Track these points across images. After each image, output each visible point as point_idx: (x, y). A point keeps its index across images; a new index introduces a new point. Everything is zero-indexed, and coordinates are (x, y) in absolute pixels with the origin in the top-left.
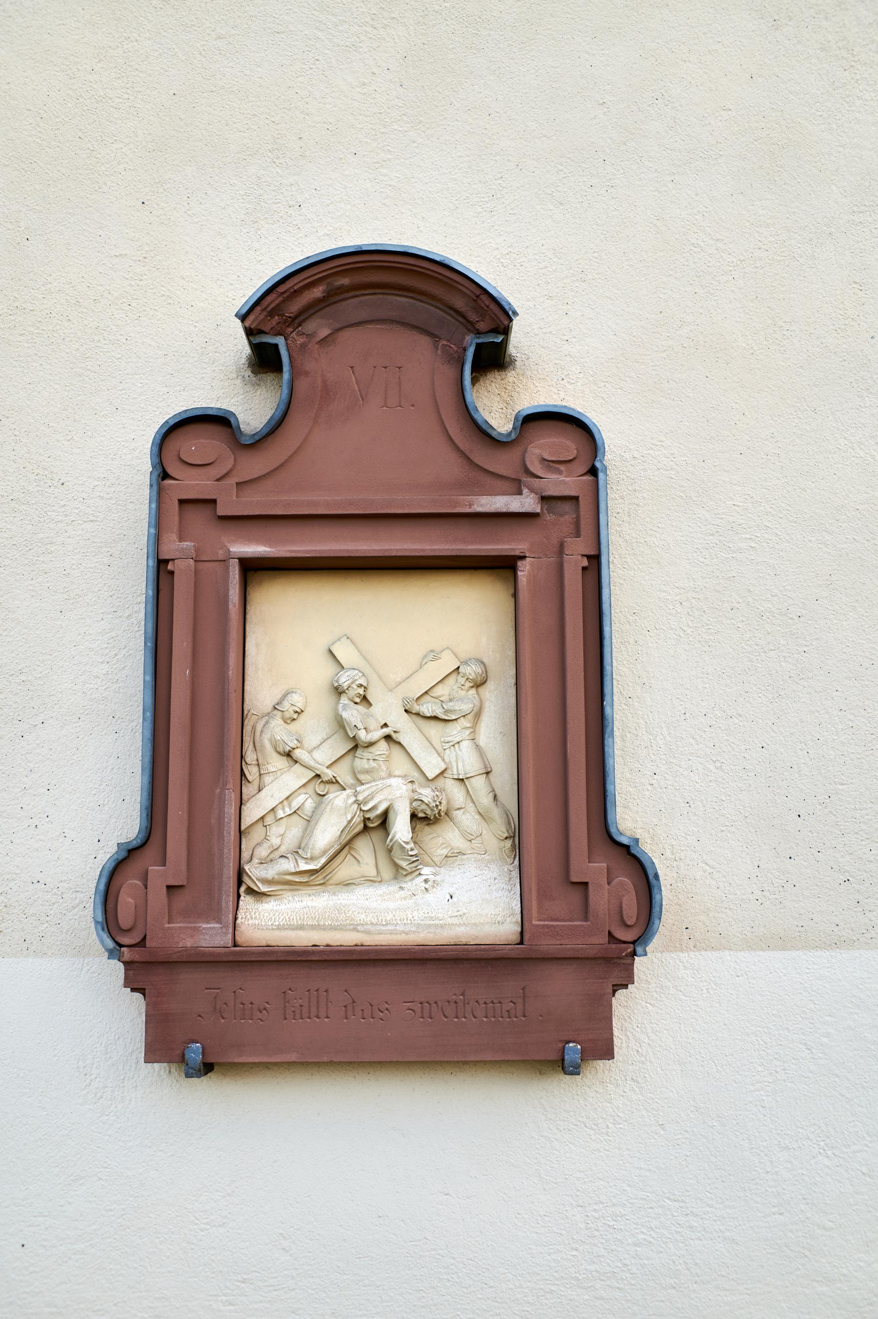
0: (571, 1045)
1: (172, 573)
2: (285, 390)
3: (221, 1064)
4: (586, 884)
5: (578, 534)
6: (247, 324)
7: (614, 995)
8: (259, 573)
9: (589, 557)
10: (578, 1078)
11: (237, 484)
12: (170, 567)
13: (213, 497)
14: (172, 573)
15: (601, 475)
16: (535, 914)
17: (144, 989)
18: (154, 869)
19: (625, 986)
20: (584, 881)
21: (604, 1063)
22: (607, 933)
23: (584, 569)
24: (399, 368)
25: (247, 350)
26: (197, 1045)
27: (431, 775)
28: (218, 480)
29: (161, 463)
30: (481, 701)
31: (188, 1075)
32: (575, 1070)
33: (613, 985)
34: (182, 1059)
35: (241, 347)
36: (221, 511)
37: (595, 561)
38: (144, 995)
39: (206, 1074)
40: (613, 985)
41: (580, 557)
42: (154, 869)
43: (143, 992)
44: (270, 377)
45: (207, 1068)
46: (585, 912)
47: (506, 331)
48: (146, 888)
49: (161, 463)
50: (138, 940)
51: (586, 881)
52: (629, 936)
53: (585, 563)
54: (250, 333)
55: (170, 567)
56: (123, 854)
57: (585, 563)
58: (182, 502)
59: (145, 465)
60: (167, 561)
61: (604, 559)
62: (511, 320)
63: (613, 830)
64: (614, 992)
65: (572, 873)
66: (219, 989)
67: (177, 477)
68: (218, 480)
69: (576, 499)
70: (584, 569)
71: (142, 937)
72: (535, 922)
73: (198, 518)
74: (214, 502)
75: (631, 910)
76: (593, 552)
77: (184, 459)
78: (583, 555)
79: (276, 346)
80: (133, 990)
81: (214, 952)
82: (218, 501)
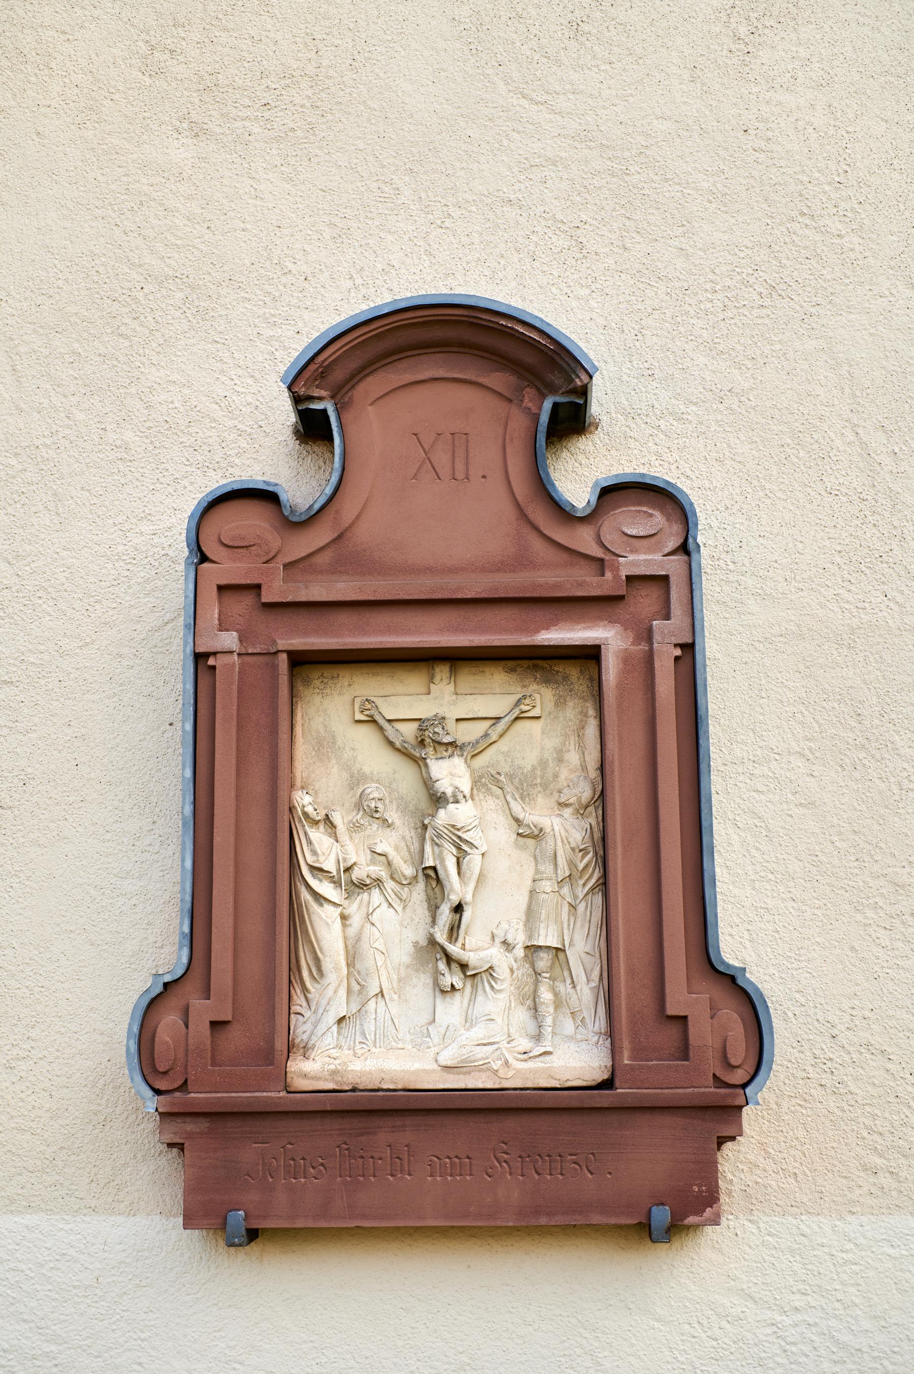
4: (685, 1018)
7: (719, 1149)
8: (306, 666)
9: (682, 646)
11: (285, 566)
12: (211, 661)
13: (256, 582)
14: (213, 668)
15: (694, 556)
16: (626, 1054)
17: (183, 1144)
18: (197, 1004)
19: (733, 1139)
20: (682, 1014)
21: (428, 984)
23: (677, 659)
25: (293, 418)
29: (199, 548)
31: (231, 1245)
33: (718, 1138)
34: (223, 1226)
35: (286, 415)
37: (689, 649)
40: (718, 1138)
42: (197, 1004)
43: (179, 1146)
44: (319, 448)
45: (253, 1235)
46: (684, 1051)
47: (584, 392)
48: (187, 1026)
49: (199, 548)
51: (686, 1014)
52: (739, 1076)
53: (678, 652)
54: (297, 400)
55: (211, 661)
56: (159, 989)
57: (678, 652)
58: (221, 588)
59: (181, 550)
61: (697, 647)
62: (591, 377)
64: (720, 1144)
65: (668, 1005)
66: (575, 1155)
69: (665, 579)
70: (677, 659)
72: (626, 1062)
73: (241, 605)
74: (258, 587)
75: (739, 1052)
76: (690, 641)
77: (224, 542)
78: (676, 645)
79: (324, 411)
80: (170, 1145)
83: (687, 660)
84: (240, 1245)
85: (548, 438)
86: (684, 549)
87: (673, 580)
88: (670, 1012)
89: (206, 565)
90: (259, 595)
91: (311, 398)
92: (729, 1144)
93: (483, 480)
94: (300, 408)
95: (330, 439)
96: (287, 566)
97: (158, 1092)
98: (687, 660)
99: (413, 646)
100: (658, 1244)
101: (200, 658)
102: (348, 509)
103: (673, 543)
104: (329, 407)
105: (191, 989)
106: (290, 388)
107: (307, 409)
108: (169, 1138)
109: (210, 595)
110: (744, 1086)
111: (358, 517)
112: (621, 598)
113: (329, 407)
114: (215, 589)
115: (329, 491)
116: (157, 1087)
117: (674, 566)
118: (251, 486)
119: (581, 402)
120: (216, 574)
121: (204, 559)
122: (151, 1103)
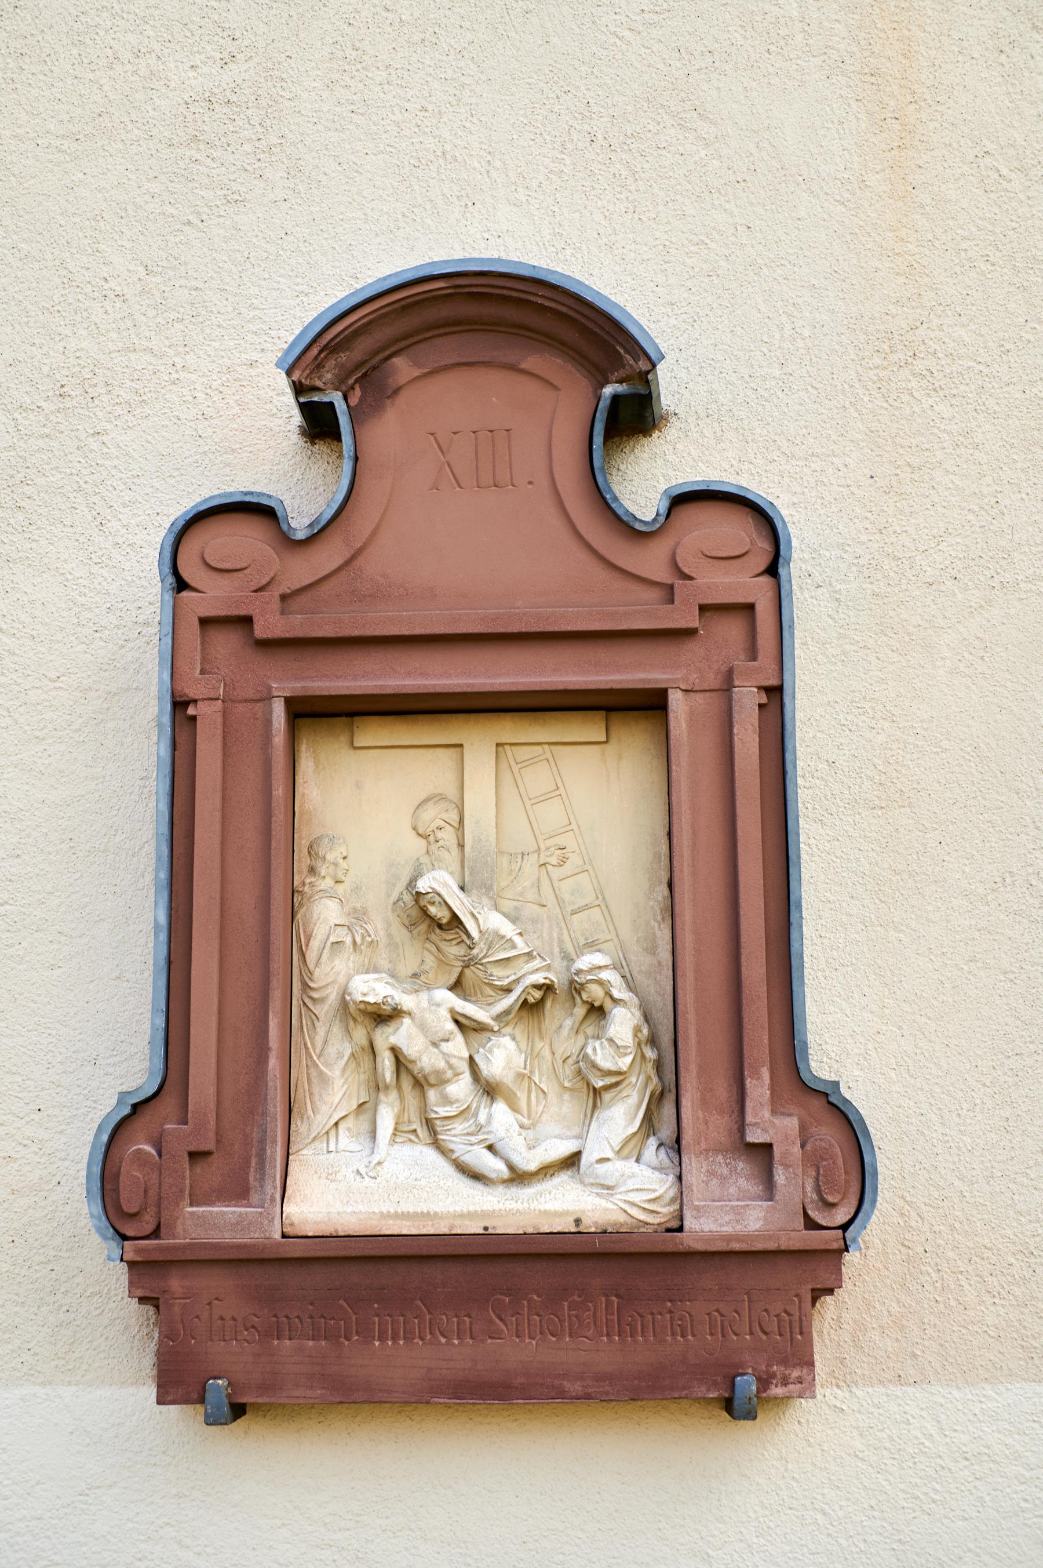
0: (211, 1381)
1: (194, 718)
2: (347, 466)
3: (257, 1407)
5: (753, 657)
6: (295, 377)
10: (747, 1424)
12: (191, 711)
14: (194, 718)
19: (830, 1291)
22: (451, 1026)
24: (507, 431)
25: (297, 418)
26: (220, 1382)
27: (605, 739)
28: (256, 591)
30: (582, 1023)
32: (751, 1415)
33: (813, 1290)
36: (260, 631)
38: (157, 1307)
39: (235, 1420)
41: (756, 690)
43: (155, 1302)
44: (321, 447)
45: (238, 1411)
50: (149, 1228)
52: (841, 1216)
53: (764, 700)
54: (299, 389)
55: (191, 711)
56: (127, 1110)
57: (764, 700)
58: (205, 622)
60: (186, 704)
62: (654, 366)
63: (804, 1075)
67: (200, 588)
68: (256, 591)
69: (750, 608)
71: (157, 1224)
73: (226, 642)
74: (246, 621)
76: (773, 682)
80: (142, 1300)
81: (240, 1243)
82: (255, 619)
83: (773, 709)
84: (226, 1424)
85: (608, 436)
86: (772, 570)
87: (759, 608)
88: (754, 1136)
89: (185, 594)
90: (252, 630)
91: (315, 389)
92: (828, 1299)
93: (530, 486)
94: (302, 400)
95: (337, 437)
96: (284, 598)
97: (124, 1238)
98: (774, 708)
99: (375, 692)
100: (742, 1422)
101: (179, 705)
102: (362, 523)
103: (763, 563)
104: (336, 398)
105: (168, 1104)
106: (289, 373)
107: (139, 1149)
108: (140, 1293)
109: (192, 630)
110: (845, 1227)
111: (374, 533)
112: (689, 633)
113: (336, 398)
114: (197, 622)
115: (340, 497)
116: (122, 1231)
117: (759, 592)
118: (687, 490)
119: (643, 391)
120: (197, 604)
121: (181, 585)
122: (114, 1248)
